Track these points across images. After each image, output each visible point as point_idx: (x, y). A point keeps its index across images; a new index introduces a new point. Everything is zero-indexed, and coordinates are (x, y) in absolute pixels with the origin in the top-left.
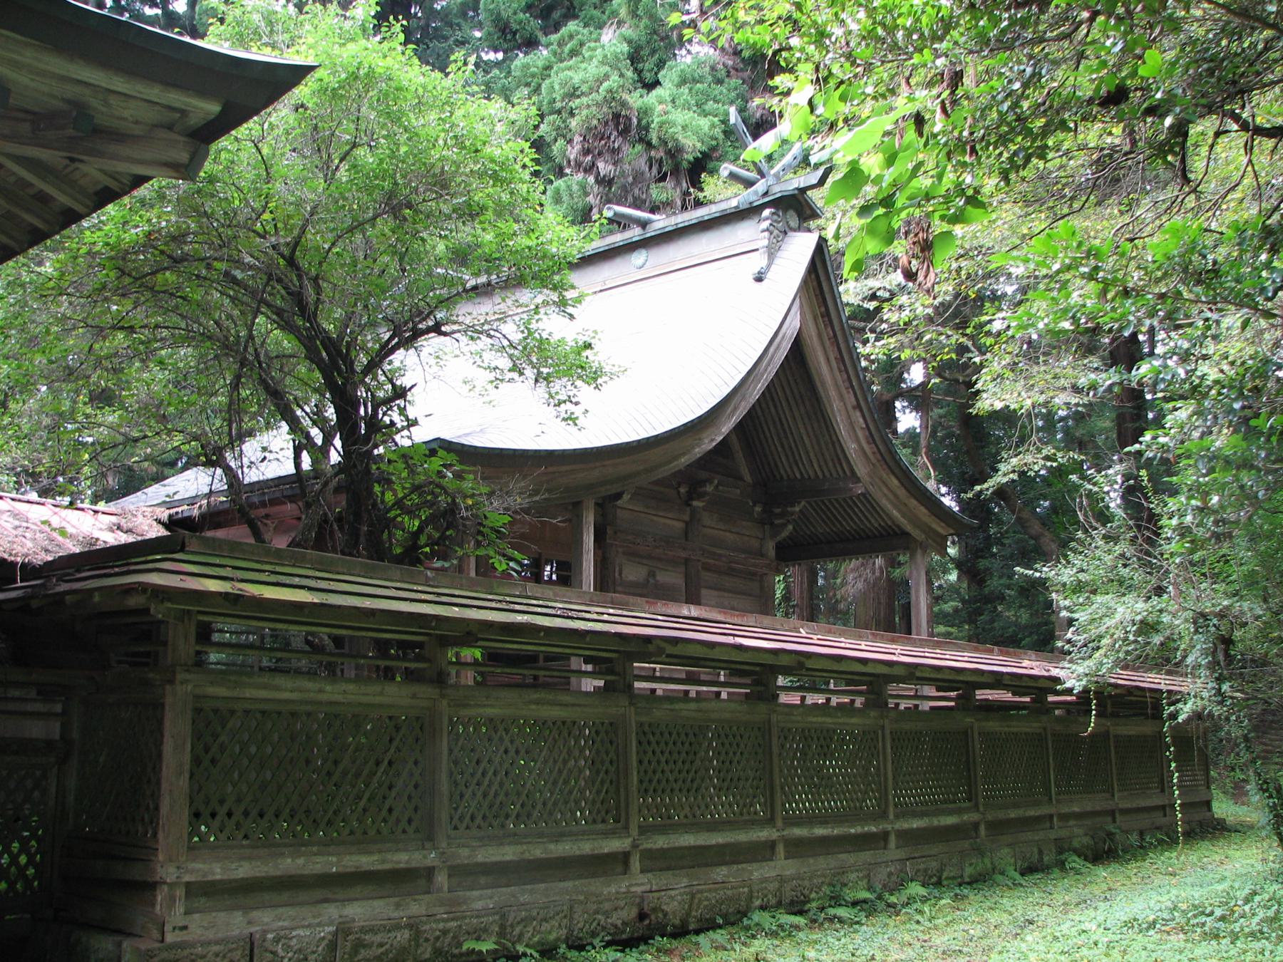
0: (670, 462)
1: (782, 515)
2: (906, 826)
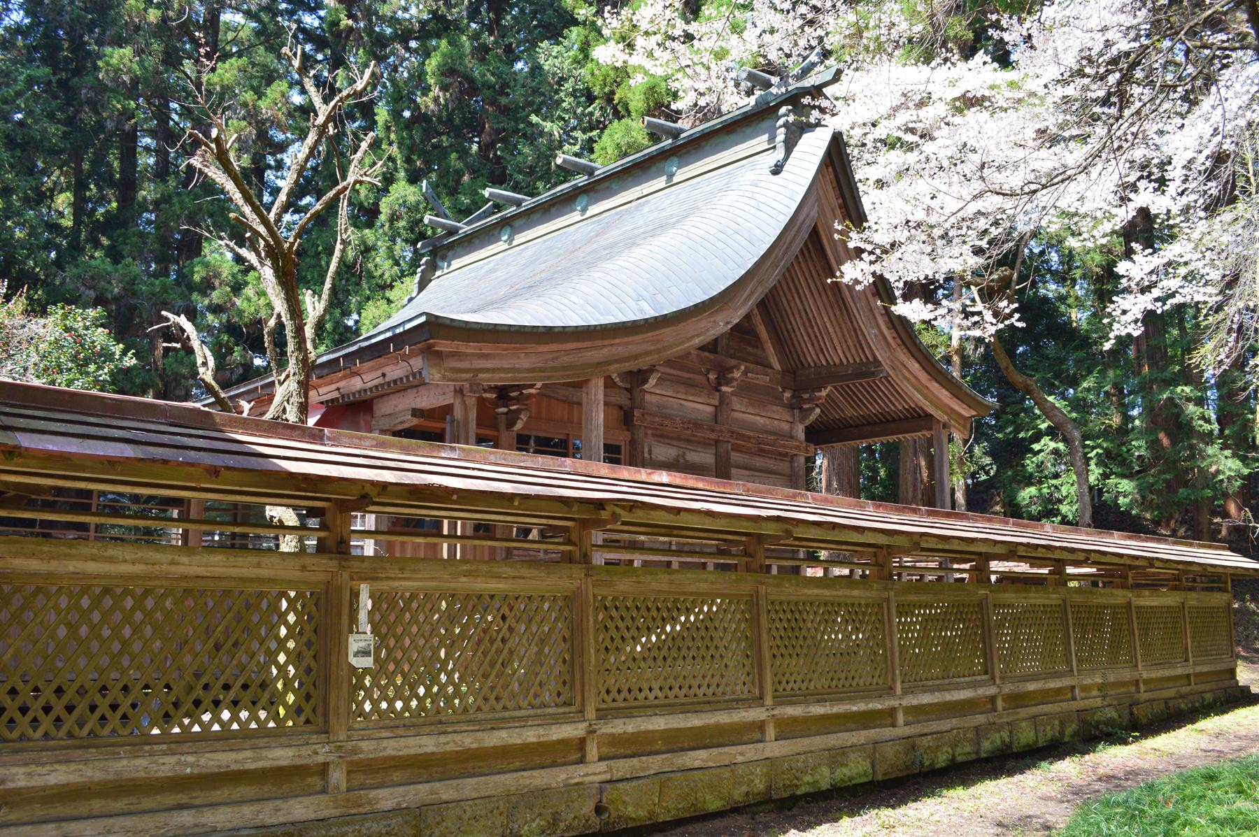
0: (682, 343)
1: (809, 400)
2: (915, 702)
